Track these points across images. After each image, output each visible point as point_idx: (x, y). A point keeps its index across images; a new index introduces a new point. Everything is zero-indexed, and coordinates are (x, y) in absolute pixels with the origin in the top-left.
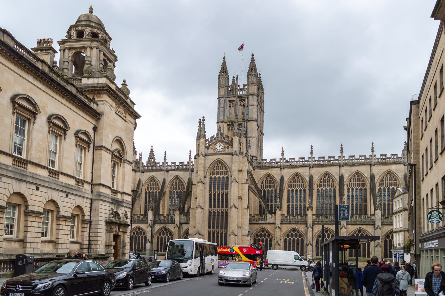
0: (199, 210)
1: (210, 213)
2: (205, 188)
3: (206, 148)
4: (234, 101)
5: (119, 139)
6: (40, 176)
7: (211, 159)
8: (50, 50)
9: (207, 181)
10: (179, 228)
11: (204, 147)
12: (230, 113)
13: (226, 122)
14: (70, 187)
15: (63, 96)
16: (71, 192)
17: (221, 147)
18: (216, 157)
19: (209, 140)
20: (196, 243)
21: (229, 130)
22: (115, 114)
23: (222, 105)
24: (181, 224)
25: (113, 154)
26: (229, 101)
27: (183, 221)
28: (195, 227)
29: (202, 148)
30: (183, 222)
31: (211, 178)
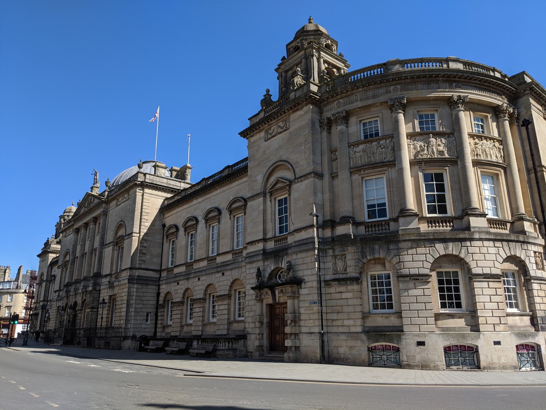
6: (200, 268)
14: (226, 264)
16: (225, 269)
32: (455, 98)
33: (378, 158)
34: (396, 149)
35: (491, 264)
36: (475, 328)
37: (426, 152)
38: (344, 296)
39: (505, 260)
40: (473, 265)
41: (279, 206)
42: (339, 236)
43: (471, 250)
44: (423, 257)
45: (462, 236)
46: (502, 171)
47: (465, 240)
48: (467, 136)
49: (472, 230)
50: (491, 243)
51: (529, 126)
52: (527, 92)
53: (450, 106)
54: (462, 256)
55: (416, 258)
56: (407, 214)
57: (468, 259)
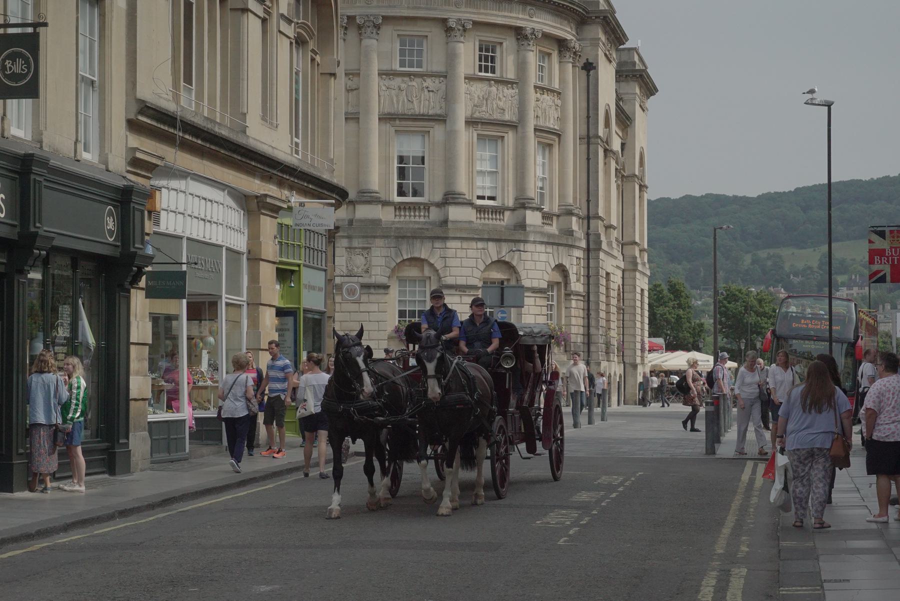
32: (529, 31)
33: (419, 108)
34: (449, 98)
35: (468, 272)
36: (142, 470)
37: (484, 108)
38: (363, 307)
39: (488, 268)
40: (523, 275)
41: (175, 127)
42: (360, 221)
43: (527, 256)
44: (472, 263)
45: (517, 237)
46: (557, 139)
47: (519, 241)
48: (532, 90)
49: (528, 229)
50: (541, 248)
51: (592, 72)
52: (598, 20)
53: (518, 39)
54: (514, 263)
55: (465, 262)
56: (460, 200)
57: (520, 269)
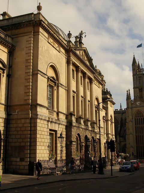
0: (131, 135)
1: (136, 136)
2: (133, 124)
3: (132, 104)
4: (141, 77)
5: (53, 64)
7: (135, 109)
8: (102, 85)
9: (134, 120)
10: (120, 144)
11: (131, 104)
12: (140, 83)
13: (138, 88)
15: (92, 88)
17: (138, 104)
18: (137, 109)
19: (133, 100)
20: (94, 171)
21: (140, 92)
22: (48, 43)
23: (135, 79)
24: (120, 142)
25: (48, 78)
26: (139, 77)
27: (122, 141)
28: (129, 144)
29: (130, 105)
30: (122, 141)
31: (135, 119)
